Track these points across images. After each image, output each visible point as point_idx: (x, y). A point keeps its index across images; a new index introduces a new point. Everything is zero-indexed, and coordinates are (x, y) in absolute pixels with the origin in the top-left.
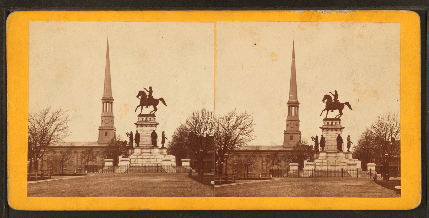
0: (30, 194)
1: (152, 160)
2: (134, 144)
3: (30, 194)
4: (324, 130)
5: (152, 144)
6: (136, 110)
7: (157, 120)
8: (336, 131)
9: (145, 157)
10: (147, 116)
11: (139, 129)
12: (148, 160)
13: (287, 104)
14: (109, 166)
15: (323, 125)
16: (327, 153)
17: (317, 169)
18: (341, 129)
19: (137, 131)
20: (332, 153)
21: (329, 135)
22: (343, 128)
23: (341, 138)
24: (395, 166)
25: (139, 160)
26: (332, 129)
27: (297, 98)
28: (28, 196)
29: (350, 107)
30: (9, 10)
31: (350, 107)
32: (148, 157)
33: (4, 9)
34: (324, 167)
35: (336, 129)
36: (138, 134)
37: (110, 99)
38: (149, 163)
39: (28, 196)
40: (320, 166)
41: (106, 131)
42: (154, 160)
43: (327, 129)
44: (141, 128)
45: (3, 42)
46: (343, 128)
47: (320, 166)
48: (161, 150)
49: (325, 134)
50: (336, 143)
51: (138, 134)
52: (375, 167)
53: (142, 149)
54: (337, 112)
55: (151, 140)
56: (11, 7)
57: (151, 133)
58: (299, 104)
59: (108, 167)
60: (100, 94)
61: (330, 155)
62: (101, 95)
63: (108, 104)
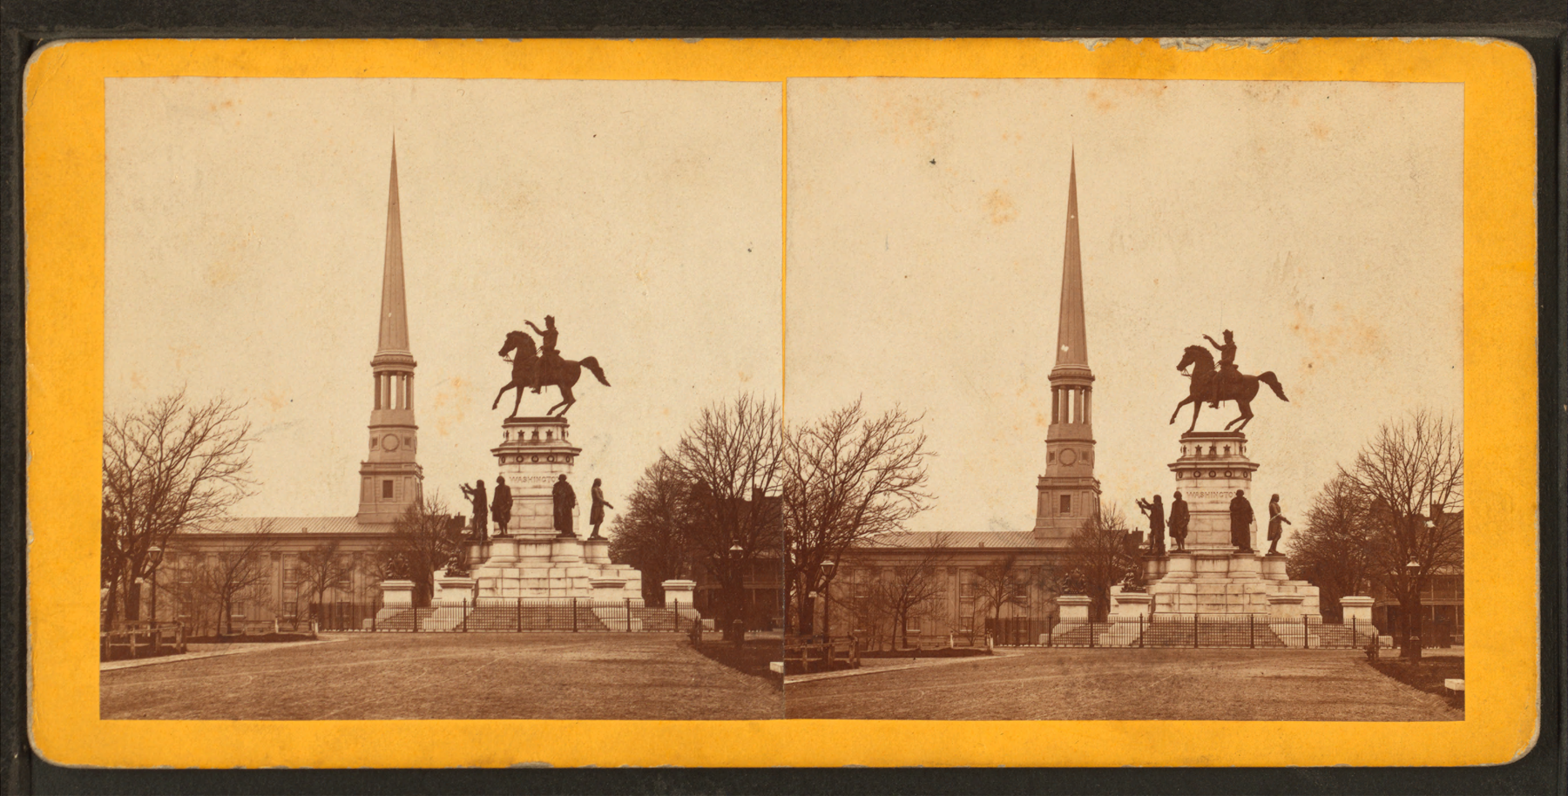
0: (109, 709)
1: (554, 584)
2: (492, 527)
3: (109, 709)
4: (508, 460)
5: (557, 526)
6: (497, 401)
7: (575, 438)
8: (1230, 478)
9: (528, 574)
10: (536, 422)
11: (510, 472)
12: (543, 584)
13: (1050, 378)
14: (398, 607)
15: (1180, 455)
16: (1196, 558)
17: (1158, 617)
18: (1248, 470)
19: (501, 480)
20: (1214, 558)
21: (1202, 495)
22: (1253, 467)
23: (1247, 503)
24: (1444, 607)
25: (507, 584)
26: (1212, 470)
27: (1085, 359)
28: (103, 716)
29: (1278, 389)
30: (33, 36)
31: (1278, 389)
32: (542, 573)
33: (13, 34)
34: (506, 593)
35: (1228, 470)
36: (503, 490)
37: (1081, 377)
38: (545, 594)
39: (103, 716)
40: (1168, 605)
41: (388, 478)
42: (561, 584)
43: (1197, 473)
44: (515, 468)
45: (11, 153)
46: (1253, 467)
47: (1168, 605)
48: (588, 548)
49: (1186, 488)
50: (1228, 523)
51: (503, 490)
52: (1369, 610)
53: (519, 543)
54: (1230, 409)
55: (551, 511)
56: (42, 27)
57: (552, 484)
58: (1093, 379)
59: (394, 611)
60: (366, 344)
61: (1206, 566)
62: (369, 348)
63: (394, 379)
